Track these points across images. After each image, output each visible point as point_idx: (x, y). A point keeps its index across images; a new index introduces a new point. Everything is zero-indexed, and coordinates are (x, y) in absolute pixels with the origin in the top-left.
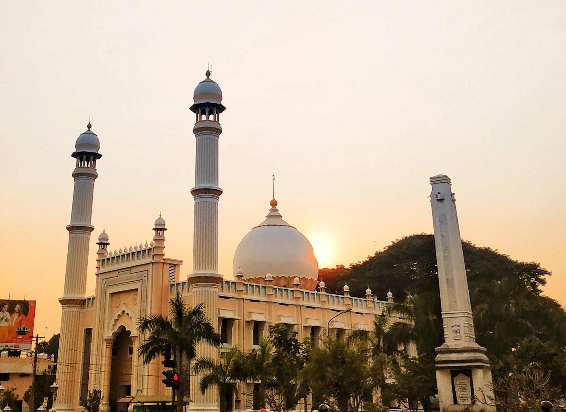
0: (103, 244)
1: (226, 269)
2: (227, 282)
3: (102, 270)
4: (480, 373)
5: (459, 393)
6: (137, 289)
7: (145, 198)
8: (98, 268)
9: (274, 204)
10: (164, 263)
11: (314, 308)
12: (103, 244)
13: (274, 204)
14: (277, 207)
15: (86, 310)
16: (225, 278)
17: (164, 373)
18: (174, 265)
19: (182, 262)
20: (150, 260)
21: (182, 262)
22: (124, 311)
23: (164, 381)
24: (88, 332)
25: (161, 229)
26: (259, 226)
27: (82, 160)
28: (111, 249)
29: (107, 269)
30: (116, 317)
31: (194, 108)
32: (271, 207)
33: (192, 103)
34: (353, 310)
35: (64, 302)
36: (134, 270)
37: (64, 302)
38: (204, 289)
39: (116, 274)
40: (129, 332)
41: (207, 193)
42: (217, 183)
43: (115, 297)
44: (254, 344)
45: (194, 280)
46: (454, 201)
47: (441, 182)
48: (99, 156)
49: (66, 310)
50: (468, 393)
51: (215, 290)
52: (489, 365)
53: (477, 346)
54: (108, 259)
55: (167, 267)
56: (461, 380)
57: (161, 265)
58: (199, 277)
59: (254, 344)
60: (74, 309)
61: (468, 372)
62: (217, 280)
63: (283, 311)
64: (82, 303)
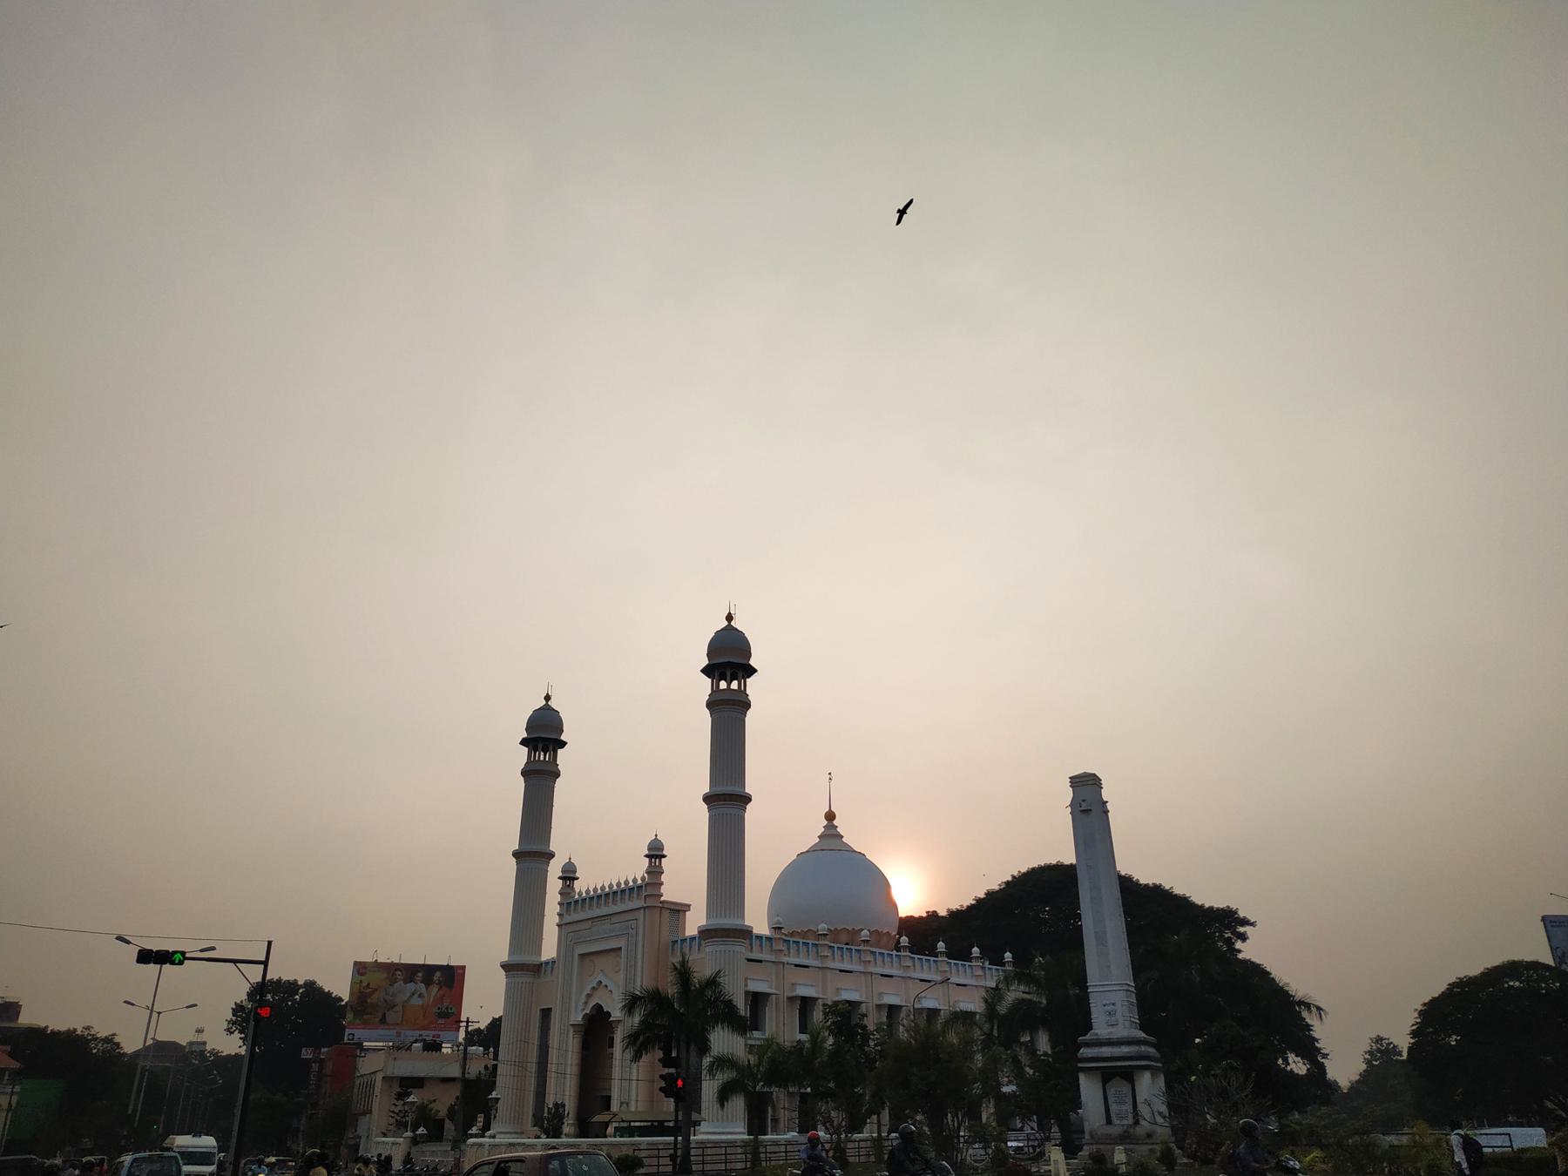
2: (759, 937)
3: (567, 919)
4: (1147, 1076)
5: (1113, 1108)
7: (632, 808)
9: (830, 816)
13: (830, 816)
16: (756, 931)
17: (662, 1077)
18: (679, 910)
20: (640, 903)
24: (546, 1013)
29: (575, 917)
35: (505, 966)
38: (722, 948)
41: (727, 799)
50: (1129, 1107)
51: (741, 949)
54: (576, 902)
55: (666, 914)
56: (1118, 1088)
60: (524, 979)
61: (1129, 1076)
62: (745, 934)
64: (537, 969)
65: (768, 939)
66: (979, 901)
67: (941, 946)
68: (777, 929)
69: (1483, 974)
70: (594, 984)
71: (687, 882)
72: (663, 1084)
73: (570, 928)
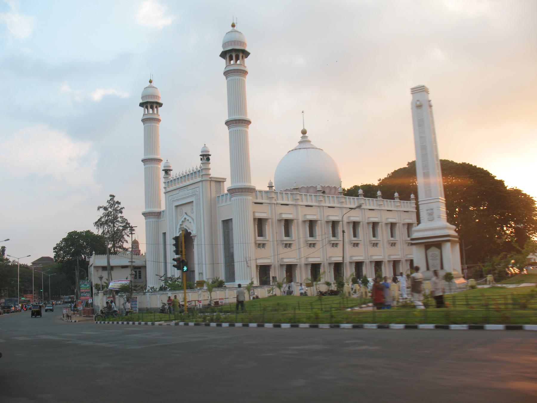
0: (167, 171)
1: (260, 183)
2: (261, 192)
3: (168, 190)
4: (448, 245)
5: (430, 262)
6: (192, 202)
7: (193, 132)
8: (165, 188)
9: (304, 132)
10: (211, 181)
11: (334, 207)
12: (167, 171)
13: (304, 132)
14: (307, 135)
15: (162, 220)
16: (258, 188)
17: (174, 260)
18: (219, 182)
19: (225, 179)
20: (199, 179)
21: (225, 179)
22: (185, 218)
23: (174, 266)
24: (164, 234)
25: (206, 155)
26: (296, 149)
27: (147, 107)
28: (173, 174)
29: (171, 188)
30: (180, 223)
31: (223, 55)
32: (302, 135)
33: (221, 50)
34: (364, 207)
35: (145, 214)
36: (189, 188)
37: (145, 214)
38: (240, 197)
39: (177, 191)
40: (190, 233)
41: (238, 123)
42: (246, 115)
43: (179, 208)
44: (285, 236)
45: (232, 191)
46: (431, 106)
47: (420, 91)
48: (160, 105)
49: (148, 220)
50: (438, 262)
51: (250, 198)
52: (457, 239)
53: (448, 225)
54: (171, 181)
55: (213, 184)
56: (434, 251)
57: (209, 183)
58: (235, 189)
59: (285, 236)
60: (152, 220)
61: (438, 245)
62: (250, 190)
63: (284, 209)
64: (159, 215)
65: (266, 192)
66: (493, 177)
67: (396, 195)
68: (270, 187)
69: (479, 168)
70: (183, 219)
71: (221, 167)
72: (175, 263)
73: (168, 194)
